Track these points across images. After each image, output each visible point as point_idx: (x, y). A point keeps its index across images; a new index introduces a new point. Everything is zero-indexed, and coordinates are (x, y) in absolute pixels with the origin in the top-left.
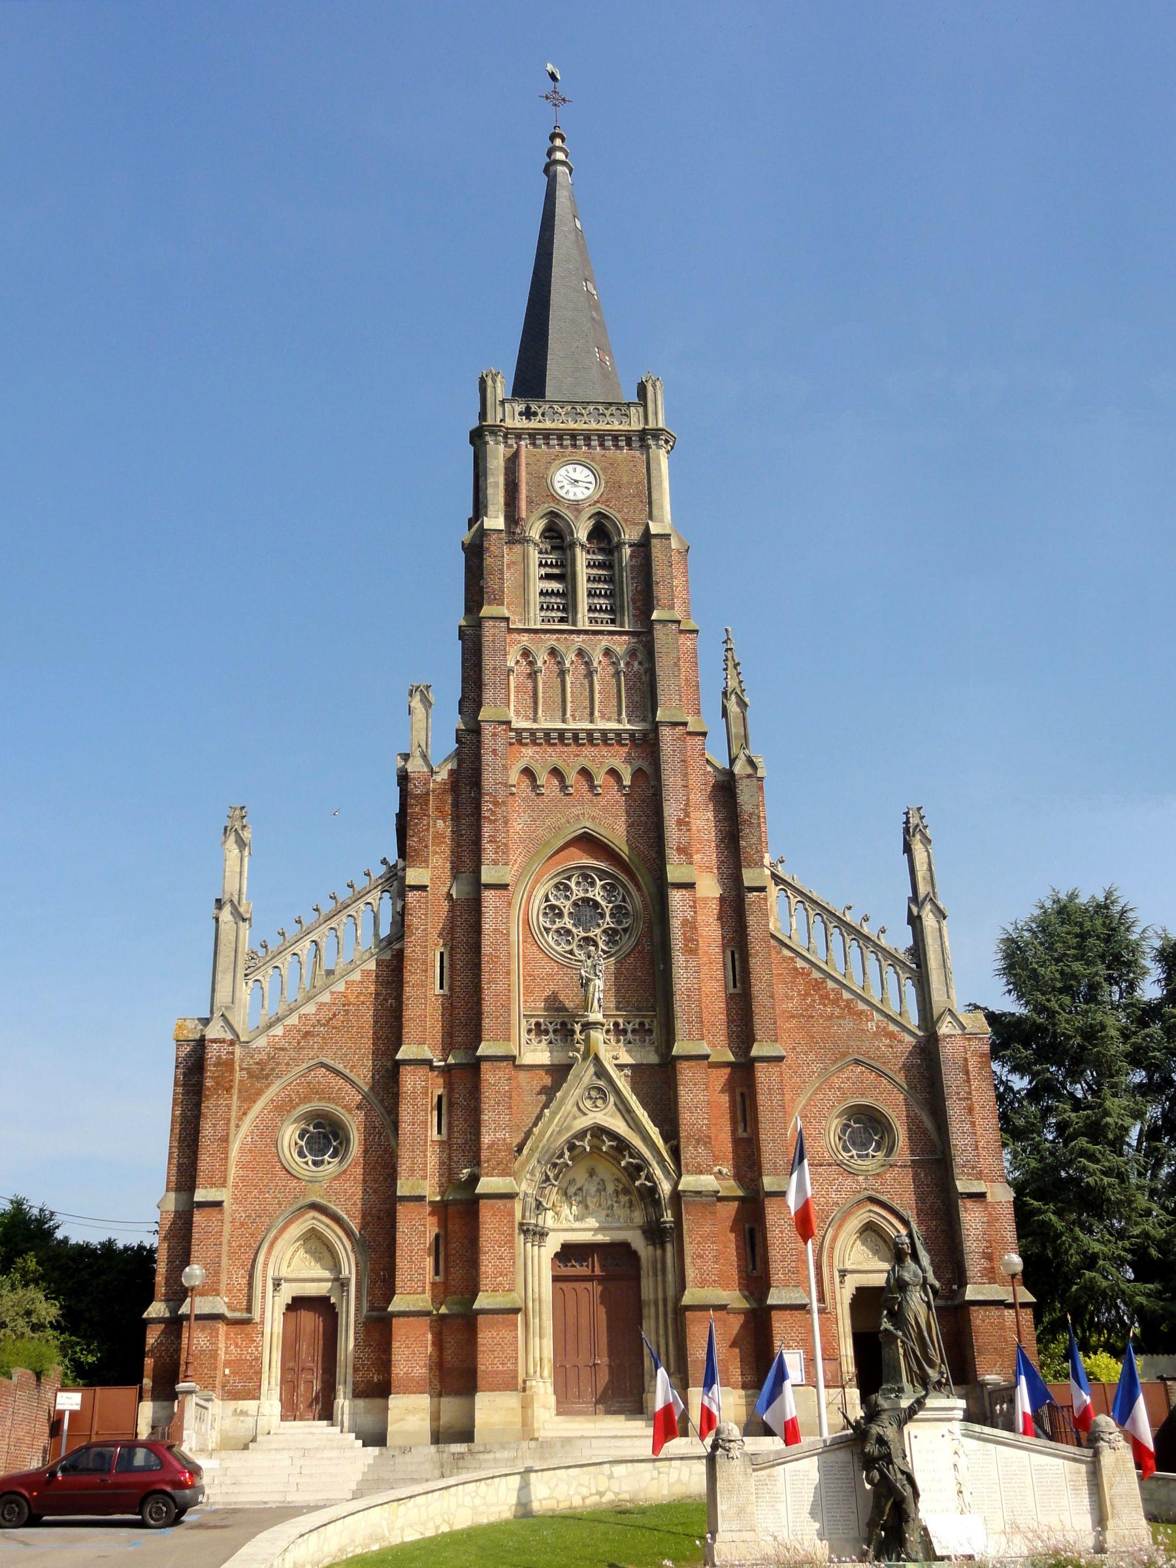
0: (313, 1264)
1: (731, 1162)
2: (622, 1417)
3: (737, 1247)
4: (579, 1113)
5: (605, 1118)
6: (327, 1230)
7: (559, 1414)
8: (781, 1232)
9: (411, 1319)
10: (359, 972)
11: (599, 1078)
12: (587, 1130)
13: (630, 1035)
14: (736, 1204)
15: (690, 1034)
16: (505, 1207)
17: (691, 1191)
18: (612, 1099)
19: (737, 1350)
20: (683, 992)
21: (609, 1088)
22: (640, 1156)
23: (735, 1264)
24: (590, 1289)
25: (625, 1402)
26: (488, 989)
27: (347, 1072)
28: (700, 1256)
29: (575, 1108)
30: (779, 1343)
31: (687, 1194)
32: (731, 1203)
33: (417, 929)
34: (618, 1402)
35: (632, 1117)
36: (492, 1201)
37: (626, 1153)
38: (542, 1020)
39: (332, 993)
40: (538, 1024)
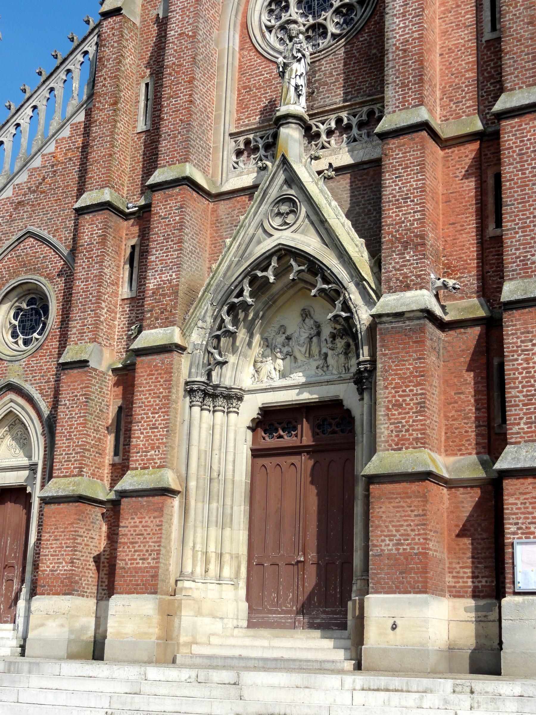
0: (17, 451)
1: (474, 272)
2: (317, 633)
3: (477, 392)
4: (264, 236)
5: (295, 235)
6: (23, 412)
7: (251, 625)
8: (527, 361)
9: (62, 506)
10: (69, 127)
11: (290, 187)
12: (270, 257)
13: (355, 131)
14: (477, 330)
15: (404, 100)
16: (163, 363)
17: (388, 315)
18: (304, 210)
19: (467, 541)
20: (397, 48)
21: (301, 197)
22: (339, 282)
23: (472, 416)
24: (298, 464)
25: (334, 613)
26: (168, 105)
27: (50, 237)
28: (398, 405)
29: (260, 231)
30: (513, 528)
31: (384, 319)
32: (469, 330)
33: (108, 60)
34: (324, 612)
35: (326, 229)
36: (150, 357)
37: (319, 278)
38: (251, 137)
39: (43, 155)
40: (247, 143)
